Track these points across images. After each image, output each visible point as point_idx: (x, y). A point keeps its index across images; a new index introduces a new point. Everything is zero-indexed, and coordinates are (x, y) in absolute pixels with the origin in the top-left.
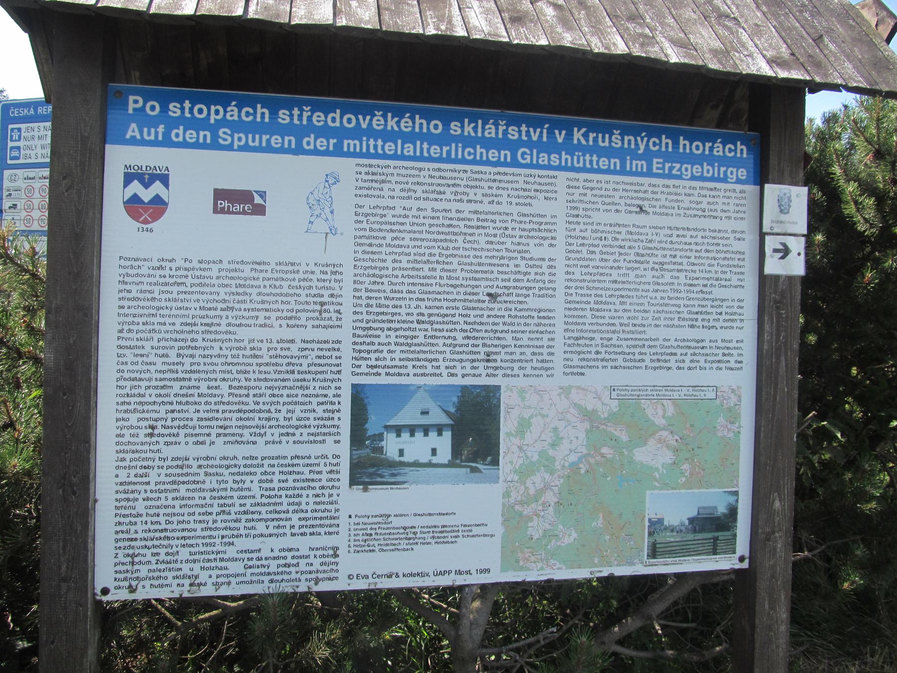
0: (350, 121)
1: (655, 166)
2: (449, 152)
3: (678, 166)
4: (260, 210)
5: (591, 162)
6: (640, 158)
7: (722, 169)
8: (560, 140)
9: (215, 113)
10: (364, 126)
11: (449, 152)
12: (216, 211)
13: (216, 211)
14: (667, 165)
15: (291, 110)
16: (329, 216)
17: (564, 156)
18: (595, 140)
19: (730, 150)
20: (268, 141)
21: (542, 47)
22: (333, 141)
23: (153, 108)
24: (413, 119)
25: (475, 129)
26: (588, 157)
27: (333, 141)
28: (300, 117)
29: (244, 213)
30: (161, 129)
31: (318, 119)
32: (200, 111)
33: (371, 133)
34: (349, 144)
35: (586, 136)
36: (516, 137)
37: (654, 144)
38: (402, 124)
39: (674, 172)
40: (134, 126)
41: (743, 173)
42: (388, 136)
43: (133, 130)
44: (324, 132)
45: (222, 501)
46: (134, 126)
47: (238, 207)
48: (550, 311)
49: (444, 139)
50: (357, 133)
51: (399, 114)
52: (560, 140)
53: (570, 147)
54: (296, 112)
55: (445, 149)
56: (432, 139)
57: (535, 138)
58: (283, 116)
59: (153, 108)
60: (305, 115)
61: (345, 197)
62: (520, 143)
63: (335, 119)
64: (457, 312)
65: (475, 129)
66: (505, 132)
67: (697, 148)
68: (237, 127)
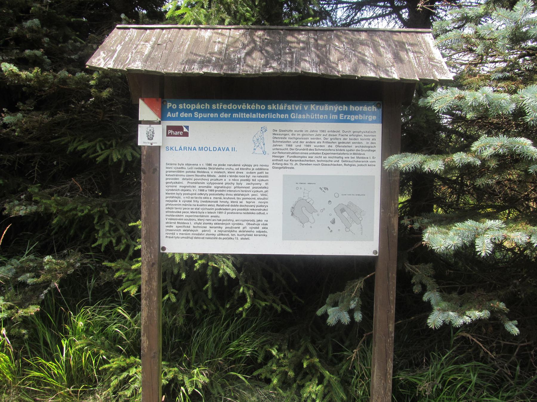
0: (235, 107)
1: (341, 116)
2: (267, 116)
3: (349, 116)
4: (186, 134)
5: (317, 117)
6: (335, 114)
7: (366, 116)
8: (306, 109)
9: (192, 107)
10: (239, 108)
11: (267, 116)
12: (168, 135)
13: (168, 135)
14: (345, 116)
15: (183, 104)
16: (263, 146)
17: (307, 115)
18: (319, 108)
19: (203, 106)
20: (209, 115)
21: (313, 74)
22: (229, 115)
23: (174, 106)
24: (246, 105)
25: (276, 107)
26: (316, 115)
27: (229, 115)
28: (219, 107)
29: (179, 136)
30: (177, 113)
31: (225, 107)
32: (188, 106)
33: (242, 111)
34: (235, 115)
35: (315, 107)
36: (290, 109)
37: (203, 106)
38: (252, 107)
39: (348, 118)
40: (169, 113)
41: (374, 118)
42: (247, 111)
43: (169, 115)
44: (227, 111)
45: (171, 228)
46: (169, 113)
47: (177, 133)
48: (266, 166)
49: (266, 111)
50: (237, 111)
51: (251, 104)
52: (306, 109)
53: (309, 111)
54: (218, 105)
55: (266, 115)
56: (261, 111)
57: (297, 109)
58: (214, 107)
59: (174, 106)
60: (221, 106)
61: (268, 137)
62: (292, 111)
63: (230, 106)
64: (239, 167)
65: (276, 107)
66: (287, 107)
67: (188, 106)
68: (200, 111)
